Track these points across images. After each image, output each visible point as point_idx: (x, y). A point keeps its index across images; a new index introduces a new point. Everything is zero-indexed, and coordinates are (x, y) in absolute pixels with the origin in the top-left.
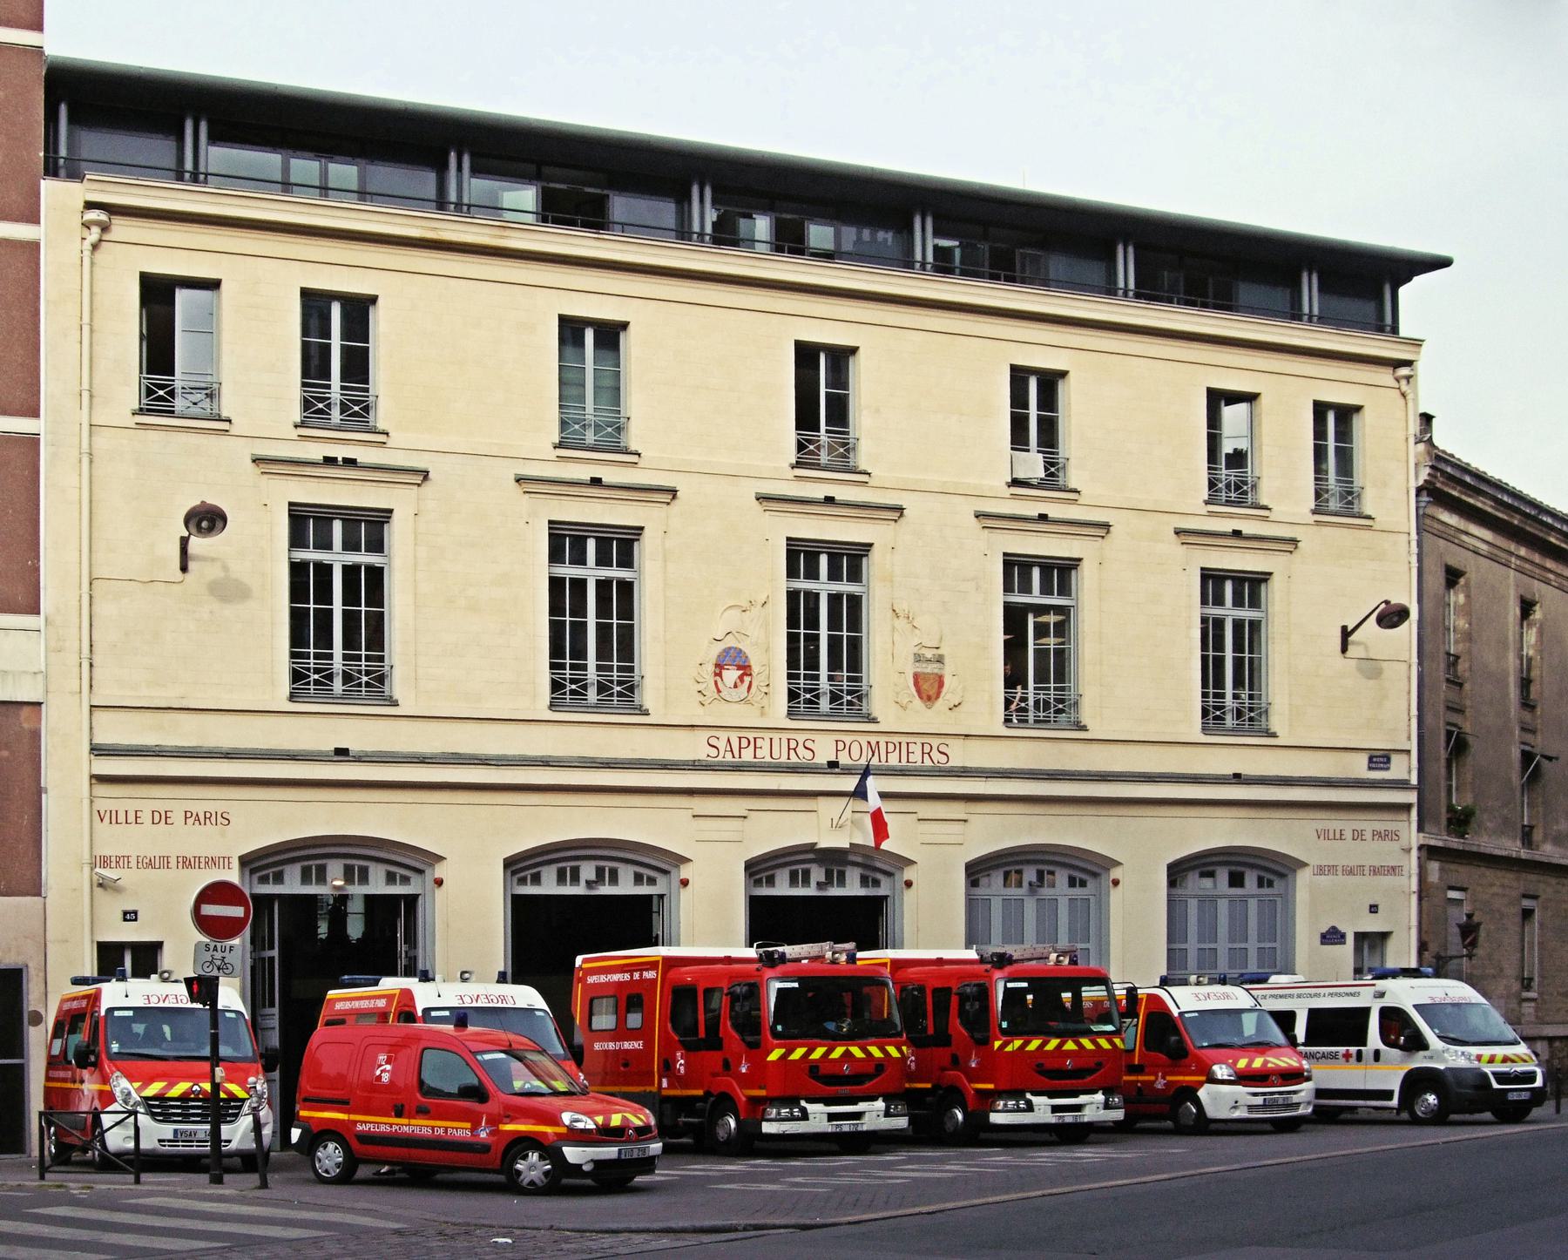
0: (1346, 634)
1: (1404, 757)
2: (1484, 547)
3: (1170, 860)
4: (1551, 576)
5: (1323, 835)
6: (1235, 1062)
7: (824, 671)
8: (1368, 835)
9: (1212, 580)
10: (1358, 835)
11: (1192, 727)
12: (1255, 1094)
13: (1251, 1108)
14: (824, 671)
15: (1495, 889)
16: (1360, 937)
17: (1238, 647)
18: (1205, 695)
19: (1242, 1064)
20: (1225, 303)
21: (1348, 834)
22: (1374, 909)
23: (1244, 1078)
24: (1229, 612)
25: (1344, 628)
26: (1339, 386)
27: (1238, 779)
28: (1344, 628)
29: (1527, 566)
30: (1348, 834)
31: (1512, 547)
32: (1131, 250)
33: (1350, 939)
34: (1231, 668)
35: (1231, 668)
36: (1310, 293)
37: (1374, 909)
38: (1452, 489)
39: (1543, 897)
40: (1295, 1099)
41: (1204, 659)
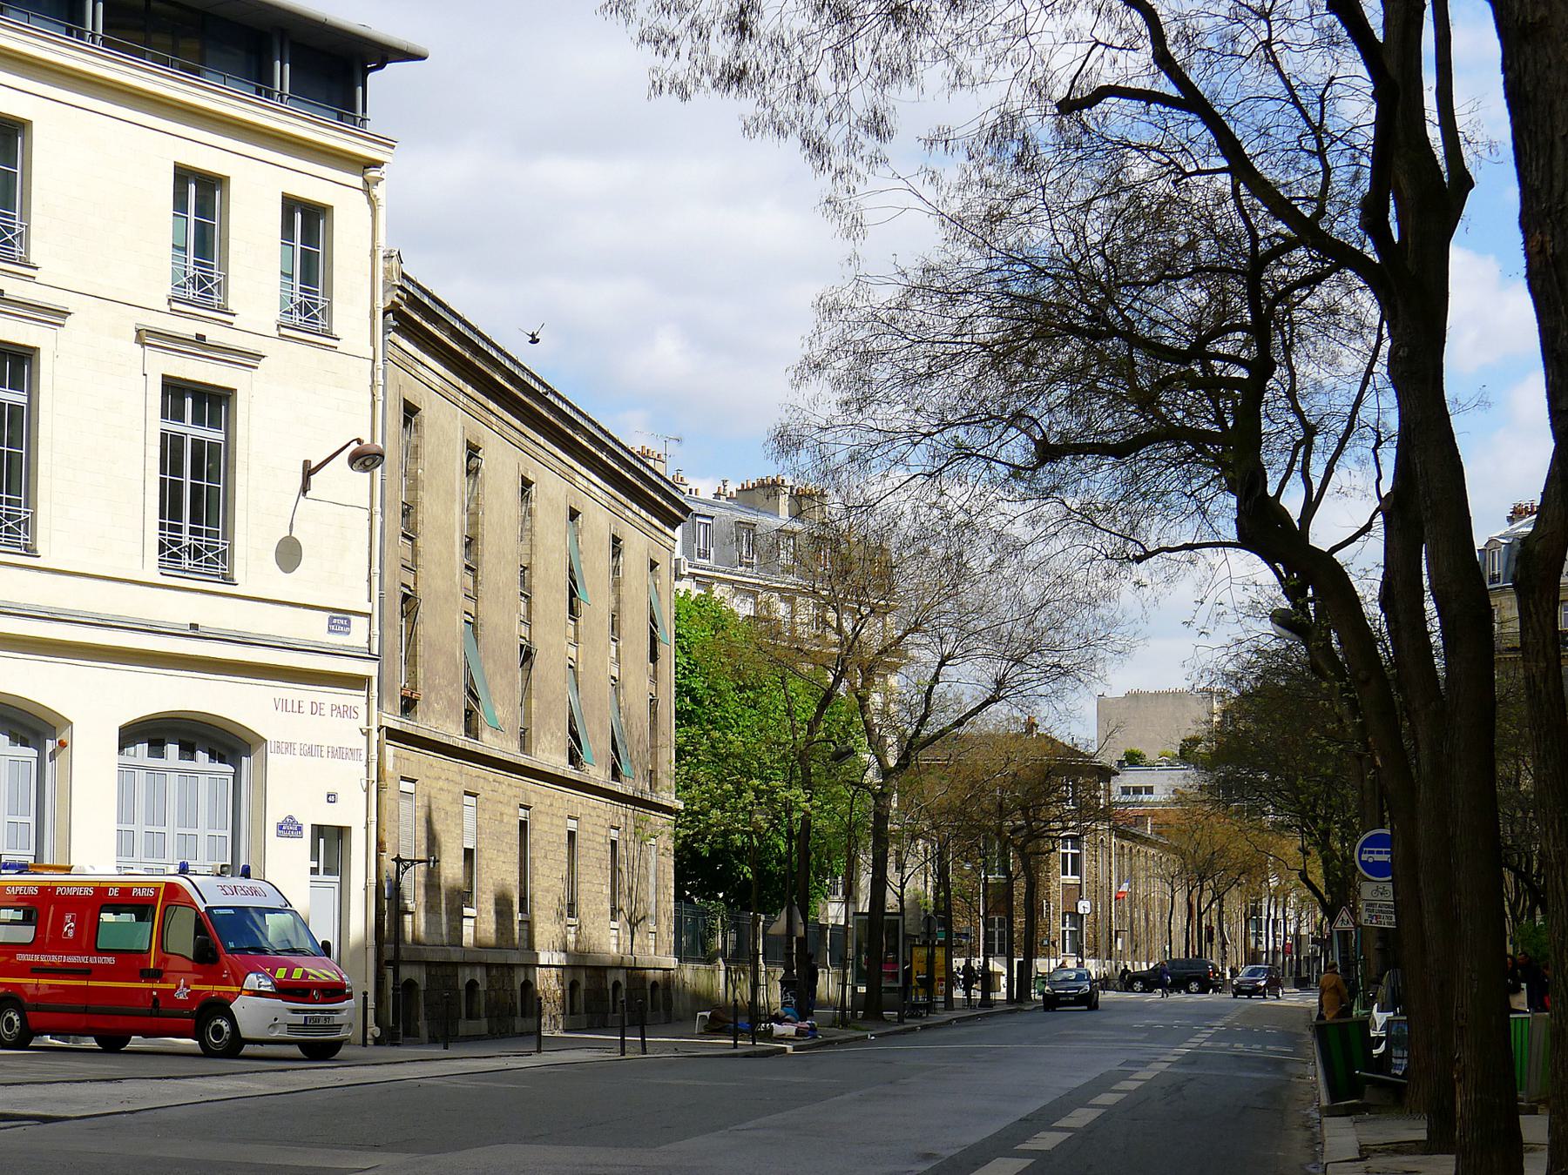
0: (309, 472)
1: (365, 620)
2: (437, 380)
3: (123, 723)
4: (493, 419)
5: (282, 705)
6: (274, 972)
7: (186, 524)
8: (327, 710)
9: (175, 390)
10: (316, 709)
11: (150, 568)
12: (295, 1011)
13: (292, 1027)
14: (186, 524)
15: (441, 783)
16: (319, 831)
17: (197, 472)
18: (162, 526)
19: (281, 973)
20: (193, 67)
21: (306, 707)
22: (331, 798)
23: (286, 991)
24: (189, 430)
25: (306, 463)
26: (315, 183)
27: (194, 631)
28: (306, 463)
29: (473, 405)
30: (306, 707)
31: (461, 383)
32: (287, 66)
33: (307, 832)
34: (194, 498)
35: (194, 498)
36: (282, 73)
37: (331, 798)
38: (415, 318)
39: (482, 795)
40: (337, 1019)
41: (163, 481)
